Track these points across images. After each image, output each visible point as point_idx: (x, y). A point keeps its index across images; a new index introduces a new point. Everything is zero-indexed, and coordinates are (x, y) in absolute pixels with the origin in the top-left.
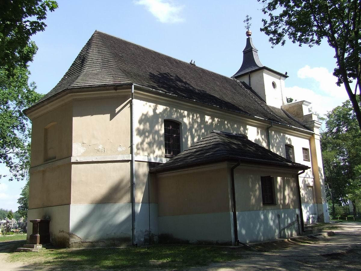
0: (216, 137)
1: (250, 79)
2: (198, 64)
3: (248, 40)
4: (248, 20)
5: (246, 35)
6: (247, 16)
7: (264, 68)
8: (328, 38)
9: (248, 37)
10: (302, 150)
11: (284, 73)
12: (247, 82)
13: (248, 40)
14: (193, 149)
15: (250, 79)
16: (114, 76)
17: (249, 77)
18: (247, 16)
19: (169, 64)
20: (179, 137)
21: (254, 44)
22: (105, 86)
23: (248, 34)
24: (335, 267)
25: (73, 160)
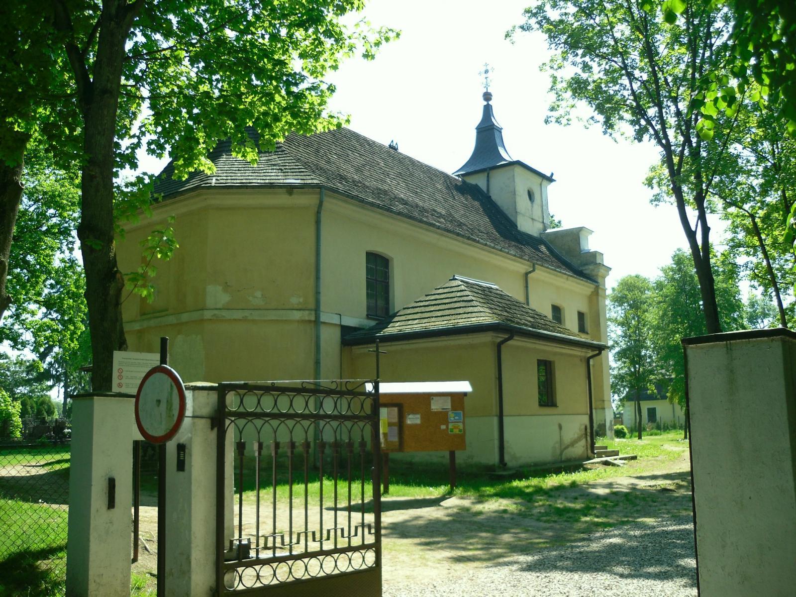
0: (463, 288)
1: (488, 181)
2: (403, 150)
3: (488, 110)
4: (487, 72)
5: (482, 98)
6: (486, 65)
7: (519, 163)
8: (159, 32)
9: (485, 103)
10: (550, 307)
11: (549, 175)
12: (483, 186)
13: (488, 110)
14: (460, 307)
15: (488, 181)
16: (283, 168)
17: (488, 176)
18: (486, 65)
19: (359, 147)
20: (388, 283)
21: (499, 119)
22: (272, 186)
23: (487, 96)
24: (598, 497)
25: (124, 321)
